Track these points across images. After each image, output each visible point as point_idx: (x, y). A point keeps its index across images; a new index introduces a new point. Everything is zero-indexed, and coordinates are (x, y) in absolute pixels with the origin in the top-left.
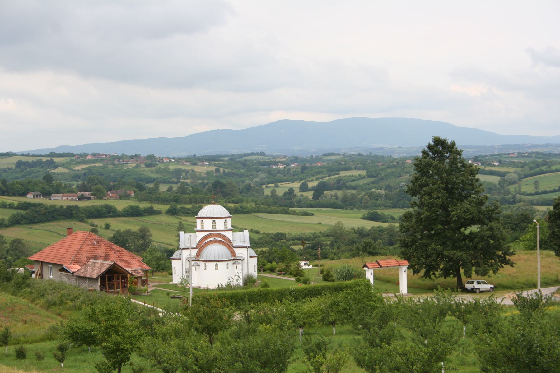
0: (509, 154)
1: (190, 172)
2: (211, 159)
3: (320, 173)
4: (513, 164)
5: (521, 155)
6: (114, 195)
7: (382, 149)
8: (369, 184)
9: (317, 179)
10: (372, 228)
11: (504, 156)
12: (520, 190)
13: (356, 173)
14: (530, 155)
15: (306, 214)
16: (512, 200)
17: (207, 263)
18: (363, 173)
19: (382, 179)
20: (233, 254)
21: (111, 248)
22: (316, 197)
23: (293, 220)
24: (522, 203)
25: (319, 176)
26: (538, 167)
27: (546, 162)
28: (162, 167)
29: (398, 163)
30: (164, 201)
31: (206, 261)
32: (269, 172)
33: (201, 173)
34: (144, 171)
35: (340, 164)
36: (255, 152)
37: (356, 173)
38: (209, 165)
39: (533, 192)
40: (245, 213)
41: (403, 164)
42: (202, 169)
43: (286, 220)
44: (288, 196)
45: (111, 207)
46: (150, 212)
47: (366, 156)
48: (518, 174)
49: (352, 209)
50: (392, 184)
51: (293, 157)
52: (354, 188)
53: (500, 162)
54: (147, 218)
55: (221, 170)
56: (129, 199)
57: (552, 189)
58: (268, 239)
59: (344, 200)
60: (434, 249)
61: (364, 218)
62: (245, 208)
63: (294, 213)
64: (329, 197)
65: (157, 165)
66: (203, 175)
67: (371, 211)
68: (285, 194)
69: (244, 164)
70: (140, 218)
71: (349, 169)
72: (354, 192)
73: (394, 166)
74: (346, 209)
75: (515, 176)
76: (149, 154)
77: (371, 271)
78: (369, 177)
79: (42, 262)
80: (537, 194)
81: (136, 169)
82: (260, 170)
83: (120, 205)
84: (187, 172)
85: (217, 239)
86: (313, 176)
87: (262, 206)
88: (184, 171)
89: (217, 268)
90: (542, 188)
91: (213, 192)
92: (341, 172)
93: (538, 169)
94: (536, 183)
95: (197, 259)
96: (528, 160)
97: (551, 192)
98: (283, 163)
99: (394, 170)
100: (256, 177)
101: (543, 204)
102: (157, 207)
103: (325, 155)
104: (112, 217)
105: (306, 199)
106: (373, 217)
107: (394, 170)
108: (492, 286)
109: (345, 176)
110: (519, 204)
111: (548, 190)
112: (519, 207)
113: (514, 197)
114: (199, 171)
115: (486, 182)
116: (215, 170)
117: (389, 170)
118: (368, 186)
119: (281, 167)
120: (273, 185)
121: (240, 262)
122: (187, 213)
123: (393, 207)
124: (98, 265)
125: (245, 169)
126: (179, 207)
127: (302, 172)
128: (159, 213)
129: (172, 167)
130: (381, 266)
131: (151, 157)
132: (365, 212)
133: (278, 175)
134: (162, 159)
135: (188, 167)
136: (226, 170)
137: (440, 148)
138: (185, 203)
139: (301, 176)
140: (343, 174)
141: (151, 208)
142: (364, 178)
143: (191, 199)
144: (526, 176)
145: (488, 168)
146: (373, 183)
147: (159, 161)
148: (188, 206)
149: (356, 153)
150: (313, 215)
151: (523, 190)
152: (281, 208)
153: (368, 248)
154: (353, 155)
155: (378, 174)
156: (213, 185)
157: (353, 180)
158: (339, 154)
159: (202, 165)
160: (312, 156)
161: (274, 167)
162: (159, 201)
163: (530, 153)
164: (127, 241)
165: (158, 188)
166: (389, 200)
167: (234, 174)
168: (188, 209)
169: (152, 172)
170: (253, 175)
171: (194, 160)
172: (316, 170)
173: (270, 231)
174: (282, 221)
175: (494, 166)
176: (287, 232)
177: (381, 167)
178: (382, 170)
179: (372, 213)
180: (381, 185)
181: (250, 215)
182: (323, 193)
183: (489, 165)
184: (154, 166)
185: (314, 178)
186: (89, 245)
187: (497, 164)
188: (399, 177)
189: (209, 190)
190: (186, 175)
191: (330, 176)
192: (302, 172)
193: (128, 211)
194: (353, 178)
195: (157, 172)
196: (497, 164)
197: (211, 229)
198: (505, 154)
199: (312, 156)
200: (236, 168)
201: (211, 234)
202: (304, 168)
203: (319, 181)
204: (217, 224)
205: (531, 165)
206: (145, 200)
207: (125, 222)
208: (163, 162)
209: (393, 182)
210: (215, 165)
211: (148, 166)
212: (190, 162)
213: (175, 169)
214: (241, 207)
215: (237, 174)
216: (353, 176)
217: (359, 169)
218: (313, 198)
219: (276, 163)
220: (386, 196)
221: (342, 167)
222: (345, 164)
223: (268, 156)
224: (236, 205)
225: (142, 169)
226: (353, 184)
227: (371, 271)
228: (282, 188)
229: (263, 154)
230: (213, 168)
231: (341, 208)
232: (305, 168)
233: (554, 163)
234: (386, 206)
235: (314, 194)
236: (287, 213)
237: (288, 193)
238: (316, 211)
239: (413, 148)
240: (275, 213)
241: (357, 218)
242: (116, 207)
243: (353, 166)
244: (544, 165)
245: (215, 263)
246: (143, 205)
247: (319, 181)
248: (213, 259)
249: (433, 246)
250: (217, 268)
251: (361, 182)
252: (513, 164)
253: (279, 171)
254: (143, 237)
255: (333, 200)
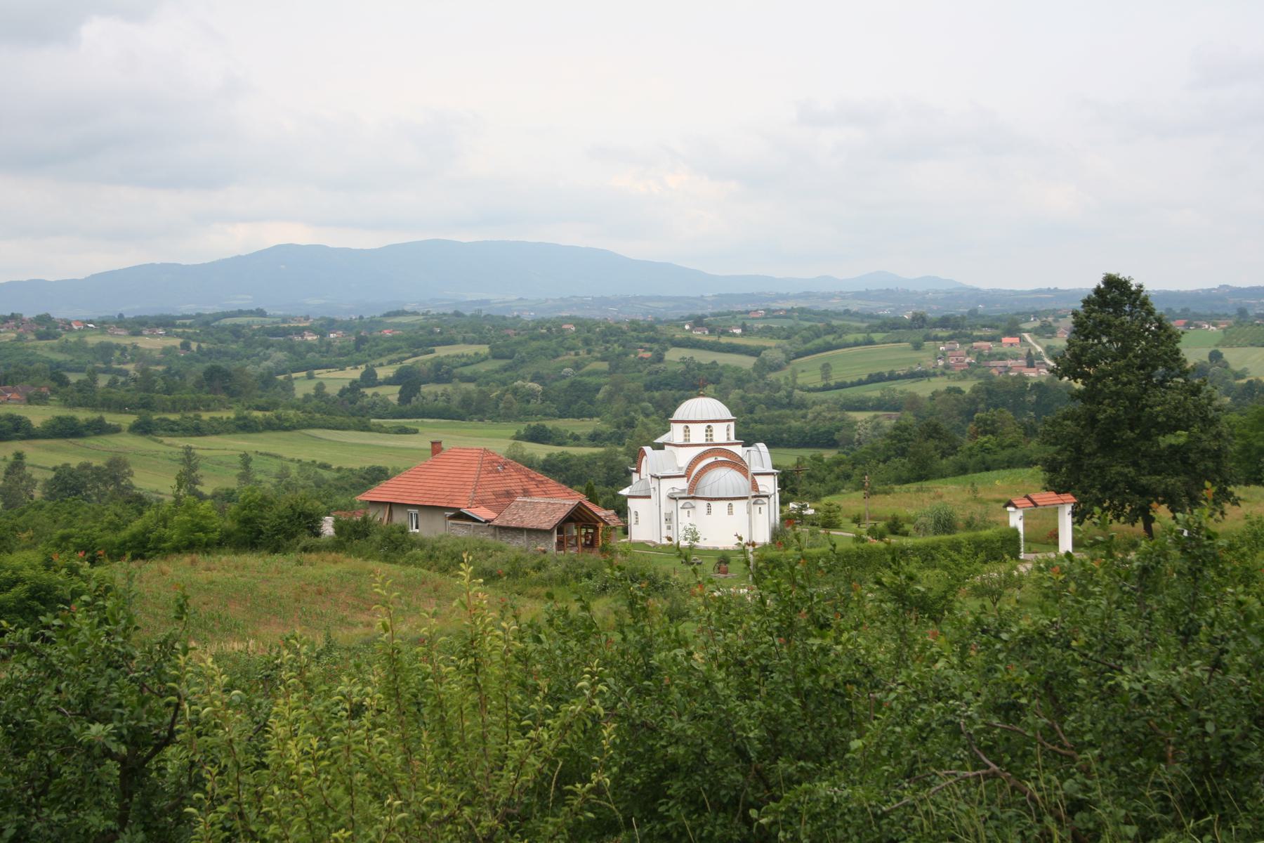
0: (748, 312)
1: (130, 348)
2: (166, 323)
3: (392, 350)
4: (768, 332)
5: (698, 322)
6: (15, 396)
7: (486, 302)
8: (497, 372)
9: (390, 363)
10: (549, 455)
11: (739, 316)
12: (794, 381)
13: (469, 350)
14: (789, 313)
15: (403, 431)
16: (786, 401)
17: (712, 503)
18: (484, 349)
19: (523, 362)
20: (755, 486)
21: (527, 476)
22: (405, 398)
23: (374, 442)
24: (824, 407)
25: (394, 356)
26: (818, 337)
27: (833, 327)
28: (73, 339)
29: (549, 329)
30: (120, 407)
31: (712, 499)
32: (291, 348)
33: (151, 350)
34: (35, 348)
35: (432, 332)
36: (244, 309)
37: (469, 350)
38: (167, 335)
39: (820, 385)
40: (286, 429)
41: (561, 331)
42: (152, 343)
43: (368, 442)
44: (349, 395)
45: (20, 418)
46: (99, 428)
47: (472, 316)
48: (784, 351)
49: (481, 420)
50: (545, 372)
51: (322, 318)
52: (470, 380)
53: (744, 327)
54: (93, 441)
55: (194, 346)
56: (47, 404)
57: (855, 379)
58: (354, 480)
59: (466, 402)
60: (1120, 474)
61: (518, 437)
62: (286, 420)
63: (380, 429)
64: (431, 398)
65: (60, 335)
66: (157, 355)
67: (533, 424)
68: (343, 392)
69: (236, 332)
70: (80, 441)
71: (450, 342)
72: (471, 387)
73: (543, 336)
74: (471, 420)
75: (779, 356)
76: (42, 312)
77: (1020, 513)
78: (495, 357)
79: (391, 504)
80: (826, 388)
81: (19, 344)
82: (272, 345)
83: (38, 416)
84: (124, 350)
85: (720, 459)
86: (381, 356)
87: (318, 416)
88: (118, 346)
89: (730, 513)
90: (835, 379)
91: (207, 388)
92: (437, 349)
93: (818, 342)
94: (826, 368)
95: (692, 495)
96: (786, 324)
97: (853, 385)
98: (310, 329)
99: (543, 343)
100: (266, 360)
101: (879, 406)
102: (111, 418)
103: (388, 315)
104: (23, 438)
105: (386, 403)
106: (538, 436)
107: (543, 343)
108: (41, 618)
109: (448, 356)
110: (818, 408)
111: (848, 381)
112: (819, 414)
113: (789, 395)
114: (147, 347)
115: (728, 366)
116: (182, 345)
117: (535, 344)
118: (497, 376)
119: (311, 338)
120: (304, 374)
121: (765, 500)
122: (172, 430)
123: (560, 417)
124: (543, 506)
125: (241, 343)
126: (155, 417)
127: (357, 349)
128: (116, 430)
129: (93, 340)
130: (1036, 505)
131: (44, 319)
132: (522, 427)
133: (309, 356)
134: (70, 324)
135: (125, 340)
136: (203, 345)
137: (1116, 295)
138: (164, 411)
139: (357, 356)
140: (442, 352)
141: (101, 420)
142: (485, 359)
143: (174, 402)
144: (798, 355)
145: (724, 340)
146: (505, 370)
147: (63, 328)
148: (173, 417)
149: (450, 311)
150: (416, 432)
151: (799, 382)
152: (355, 420)
153: (788, 482)
154: (444, 314)
155: (513, 352)
156: (205, 374)
157: (465, 365)
158: (415, 313)
159: (152, 336)
160: (361, 317)
161: (298, 339)
162: (109, 407)
163: (787, 311)
164: (84, 485)
165: (94, 381)
166: (552, 401)
167: (219, 352)
168: (174, 422)
169: (52, 349)
170: (257, 355)
171: (138, 326)
172: (386, 345)
173: (356, 466)
174: (364, 445)
175: (734, 335)
176: (390, 467)
177: (517, 338)
178: (519, 343)
179: (534, 428)
180: (521, 372)
181: (295, 433)
182: (418, 390)
183: (724, 333)
184: (55, 338)
185: (384, 360)
186: (490, 472)
187: (738, 331)
188: (554, 357)
189: (199, 385)
190: (122, 354)
191: (415, 355)
192: (357, 349)
193: (54, 427)
194: (464, 360)
195: (64, 349)
196: (738, 331)
197: (704, 442)
198: (741, 313)
199: (361, 317)
200: (221, 342)
201: (710, 451)
202: (361, 341)
203: (398, 366)
204: (714, 433)
205: (805, 333)
206: (80, 405)
207: (52, 450)
208: (71, 330)
209: (545, 366)
210: (178, 336)
211: (41, 337)
212: (126, 328)
213: (101, 343)
214: (278, 418)
215: (226, 354)
216: (463, 356)
217: (472, 343)
218: (399, 399)
219: (300, 331)
220: (546, 396)
221: (438, 338)
222: (441, 333)
223: (270, 316)
224: (268, 414)
225: (30, 344)
226: (467, 371)
227: (1020, 513)
228: (336, 380)
229: (260, 313)
230: (177, 342)
231: (461, 418)
232: (362, 340)
233: (848, 330)
234: (546, 415)
235: (401, 392)
236: (366, 428)
237: (348, 390)
238: (423, 424)
239: (547, 300)
240: (344, 429)
241: (504, 437)
242: (30, 418)
243: (460, 337)
244: (829, 333)
245: (727, 503)
246: (83, 415)
247: (398, 366)
248: (704, 499)
249: (1118, 468)
250: (730, 513)
251: (483, 368)
252: (768, 332)
253: (310, 347)
254: (115, 479)
255: (441, 404)
